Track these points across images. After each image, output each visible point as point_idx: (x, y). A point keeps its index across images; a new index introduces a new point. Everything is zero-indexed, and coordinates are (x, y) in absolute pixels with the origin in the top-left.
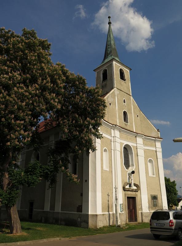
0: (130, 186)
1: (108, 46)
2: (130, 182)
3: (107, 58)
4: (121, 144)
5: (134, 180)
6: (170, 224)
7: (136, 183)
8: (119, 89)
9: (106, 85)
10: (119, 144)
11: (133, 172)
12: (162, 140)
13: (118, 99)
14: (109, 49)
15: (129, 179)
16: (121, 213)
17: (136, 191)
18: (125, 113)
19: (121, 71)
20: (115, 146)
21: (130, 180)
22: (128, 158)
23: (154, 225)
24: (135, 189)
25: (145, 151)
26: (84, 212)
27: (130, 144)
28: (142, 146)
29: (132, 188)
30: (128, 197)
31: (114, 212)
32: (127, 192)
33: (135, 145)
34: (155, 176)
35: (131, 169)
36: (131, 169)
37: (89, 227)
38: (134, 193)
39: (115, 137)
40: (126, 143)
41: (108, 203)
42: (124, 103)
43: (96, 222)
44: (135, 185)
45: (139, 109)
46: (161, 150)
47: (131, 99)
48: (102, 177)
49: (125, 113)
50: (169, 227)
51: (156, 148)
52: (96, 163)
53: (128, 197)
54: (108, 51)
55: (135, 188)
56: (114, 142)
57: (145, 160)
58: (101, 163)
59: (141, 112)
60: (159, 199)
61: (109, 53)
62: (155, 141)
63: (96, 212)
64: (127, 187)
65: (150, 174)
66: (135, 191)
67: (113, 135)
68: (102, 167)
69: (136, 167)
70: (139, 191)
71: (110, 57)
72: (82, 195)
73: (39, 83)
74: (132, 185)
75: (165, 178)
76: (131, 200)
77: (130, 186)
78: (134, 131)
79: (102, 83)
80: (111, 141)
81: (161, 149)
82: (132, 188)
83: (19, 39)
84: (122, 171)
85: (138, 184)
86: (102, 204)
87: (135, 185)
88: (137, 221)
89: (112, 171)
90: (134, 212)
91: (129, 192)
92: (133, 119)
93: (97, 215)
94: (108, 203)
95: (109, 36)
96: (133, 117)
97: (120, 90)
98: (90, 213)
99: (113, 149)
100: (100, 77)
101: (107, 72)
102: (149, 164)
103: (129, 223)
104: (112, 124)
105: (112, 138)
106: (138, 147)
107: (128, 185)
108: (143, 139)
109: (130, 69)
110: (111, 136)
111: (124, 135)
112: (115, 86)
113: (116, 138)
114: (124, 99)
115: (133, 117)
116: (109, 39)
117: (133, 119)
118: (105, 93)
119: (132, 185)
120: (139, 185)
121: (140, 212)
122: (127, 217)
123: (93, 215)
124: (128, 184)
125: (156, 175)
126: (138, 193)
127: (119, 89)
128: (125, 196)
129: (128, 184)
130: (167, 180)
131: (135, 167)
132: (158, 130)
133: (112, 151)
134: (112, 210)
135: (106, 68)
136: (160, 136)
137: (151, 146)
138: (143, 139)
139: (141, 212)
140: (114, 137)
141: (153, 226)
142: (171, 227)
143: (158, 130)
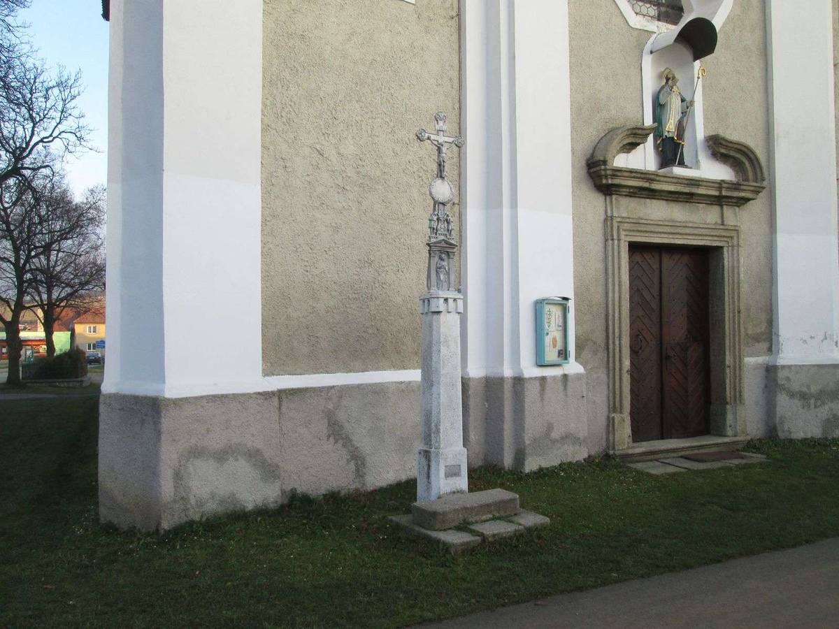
0: (670, 151)
2: (670, 127)
5: (712, 112)
7: (734, 134)
16: (543, 379)
17: (723, 197)
24: (720, 184)
29: (678, 171)
30: (634, 247)
32: (626, 207)
38: (710, 215)
44: (720, 148)
53: (634, 247)
55: (714, 171)
64: (644, 158)
66: (719, 201)
70: (756, 207)
73: (55, 295)
76: (653, 261)
77: (670, 151)
83: (504, 573)
85: (755, 143)
87: (720, 148)
88: (725, 436)
90: (648, 230)
91: (657, 211)
100: (704, 94)
103: (643, 447)
120: (762, 158)
121: (753, 361)
122: (614, 407)
126: (746, 220)
128: (608, 238)
139: (761, 360)
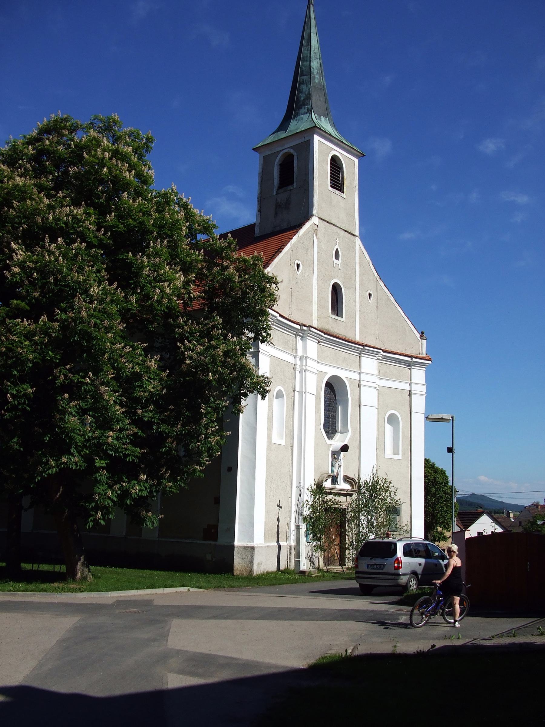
0: (335, 480)
1: (301, 75)
3: (296, 115)
4: (320, 374)
6: (396, 565)
7: (353, 475)
8: (325, 220)
9: (288, 202)
10: (315, 377)
11: (345, 448)
12: (430, 362)
13: (319, 248)
14: (304, 88)
15: (332, 466)
18: (336, 290)
19: (336, 164)
20: (304, 382)
21: (336, 466)
22: (335, 411)
23: (363, 567)
24: (347, 491)
25: (382, 391)
26: (221, 541)
27: (343, 374)
28: (375, 379)
31: (293, 544)
33: (356, 377)
34: (400, 457)
35: (337, 442)
36: (337, 442)
37: (235, 573)
39: (306, 358)
40: (331, 372)
41: (278, 526)
42: (336, 261)
43: (252, 562)
44: (347, 479)
45: (376, 275)
46: (423, 389)
47: (357, 247)
48: (268, 460)
49: (336, 290)
50: (392, 571)
51: (410, 385)
52: (256, 429)
54: (300, 92)
56: (300, 372)
57: (378, 416)
58: (268, 425)
59: (382, 284)
60: (403, 513)
61: (304, 100)
62: (409, 365)
63: (252, 539)
65: (389, 452)
67: (300, 353)
68: (270, 437)
69: (354, 433)
71: (305, 113)
72: (217, 501)
74: (340, 479)
75: (427, 461)
77: (335, 480)
78: (357, 339)
79: (277, 194)
80: (295, 369)
81: (425, 387)
82: (337, 487)
84: (316, 444)
86: (265, 523)
89: (292, 447)
92: (357, 304)
93: (253, 548)
94: (278, 526)
95: (305, 43)
96: (357, 299)
97: (328, 222)
98: (237, 543)
99: (298, 388)
101: (295, 165)
102: (388, 428)
104: (300, 325)
105: (298, 359)
106: (362, 383)
107: (330, 480)
108: (378, 359)
109: (361, 156)
110: (295, 357)
111: (330, 351)
112: (315, 212)
113: (307, 372)
114: (337, 247)
115: (357, 299)
116: (304, 52)
117: (357, 304)
118: (285, 226)
119: (338, 479)
123: (245, 548)
124: (329, 477)
125: (403, 454)
127: (325, 220)
129: (329, 477)
130: (429, 466)
131: (350, 434)
132: (422, 333)
133: (296, 393)
134: (287, 538)
135: (292, 151)
136: (424, 351)
137: (398, 379)
138: (378, 359)
140: (303, 358)
141: (360, 569)
142: (396, 571)
143: (422, 333)
